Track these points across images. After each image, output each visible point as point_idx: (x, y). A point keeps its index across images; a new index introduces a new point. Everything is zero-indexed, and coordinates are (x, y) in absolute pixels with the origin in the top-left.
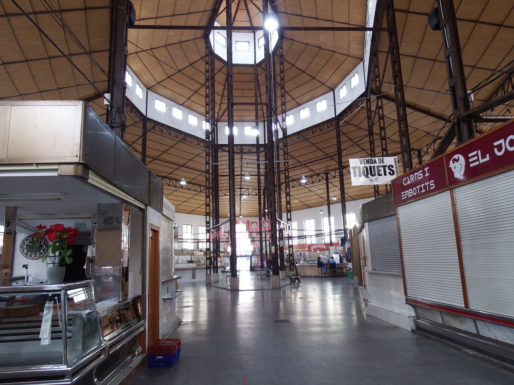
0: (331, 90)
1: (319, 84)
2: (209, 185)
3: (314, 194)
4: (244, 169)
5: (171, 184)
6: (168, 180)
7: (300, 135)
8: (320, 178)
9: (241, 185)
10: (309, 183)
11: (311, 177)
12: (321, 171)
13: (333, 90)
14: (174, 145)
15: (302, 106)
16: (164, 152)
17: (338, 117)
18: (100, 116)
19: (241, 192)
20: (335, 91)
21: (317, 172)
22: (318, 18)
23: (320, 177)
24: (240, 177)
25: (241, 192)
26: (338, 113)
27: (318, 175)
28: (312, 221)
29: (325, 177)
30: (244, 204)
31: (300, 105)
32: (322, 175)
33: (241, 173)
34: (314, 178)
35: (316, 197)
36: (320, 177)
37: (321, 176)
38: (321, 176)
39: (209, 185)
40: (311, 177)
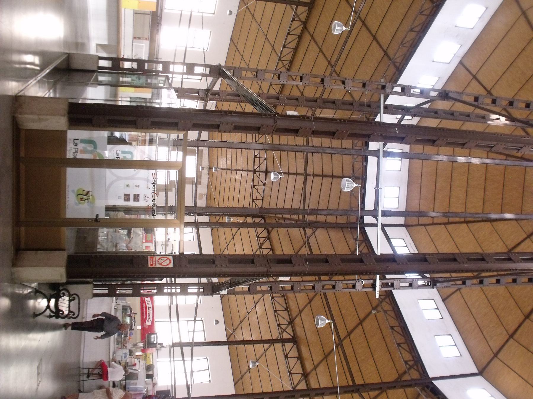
0: (480, 369)
1: (495, 345)
2: (390, 110)
3: (250, 307)
4: (317, 180)
5: (290, 38)
6: (298, 32)
7: (385, 299)
8: (284, 327)
9: (314, 175)
10: (273, 301)
11: (286, 309)
12: (299, 330)
13: (481, 373)
14: (378, 42)
15: (442, 305)
16: (236, 47)
17: (431, 386)
18: (135, 13)
19: (260, 172)
20: (480, 378)
21: (297, 321)
22: (527, 320)
23: (285, 326)
24: (301, 170)
25: (260, 172)
26: (439, 384)
27: (291, 322)
28: (177, 292)
29: (286, 336)
30: (233, 177)
31: (444, 300)
32: (289, 330)
33: (310, 175)
34: (285, 314)
35: (243, 312)
36: (285, 326)
37: (286, 328)
38: (286, 328)
39: (390, 110)
40: (286, 309)
